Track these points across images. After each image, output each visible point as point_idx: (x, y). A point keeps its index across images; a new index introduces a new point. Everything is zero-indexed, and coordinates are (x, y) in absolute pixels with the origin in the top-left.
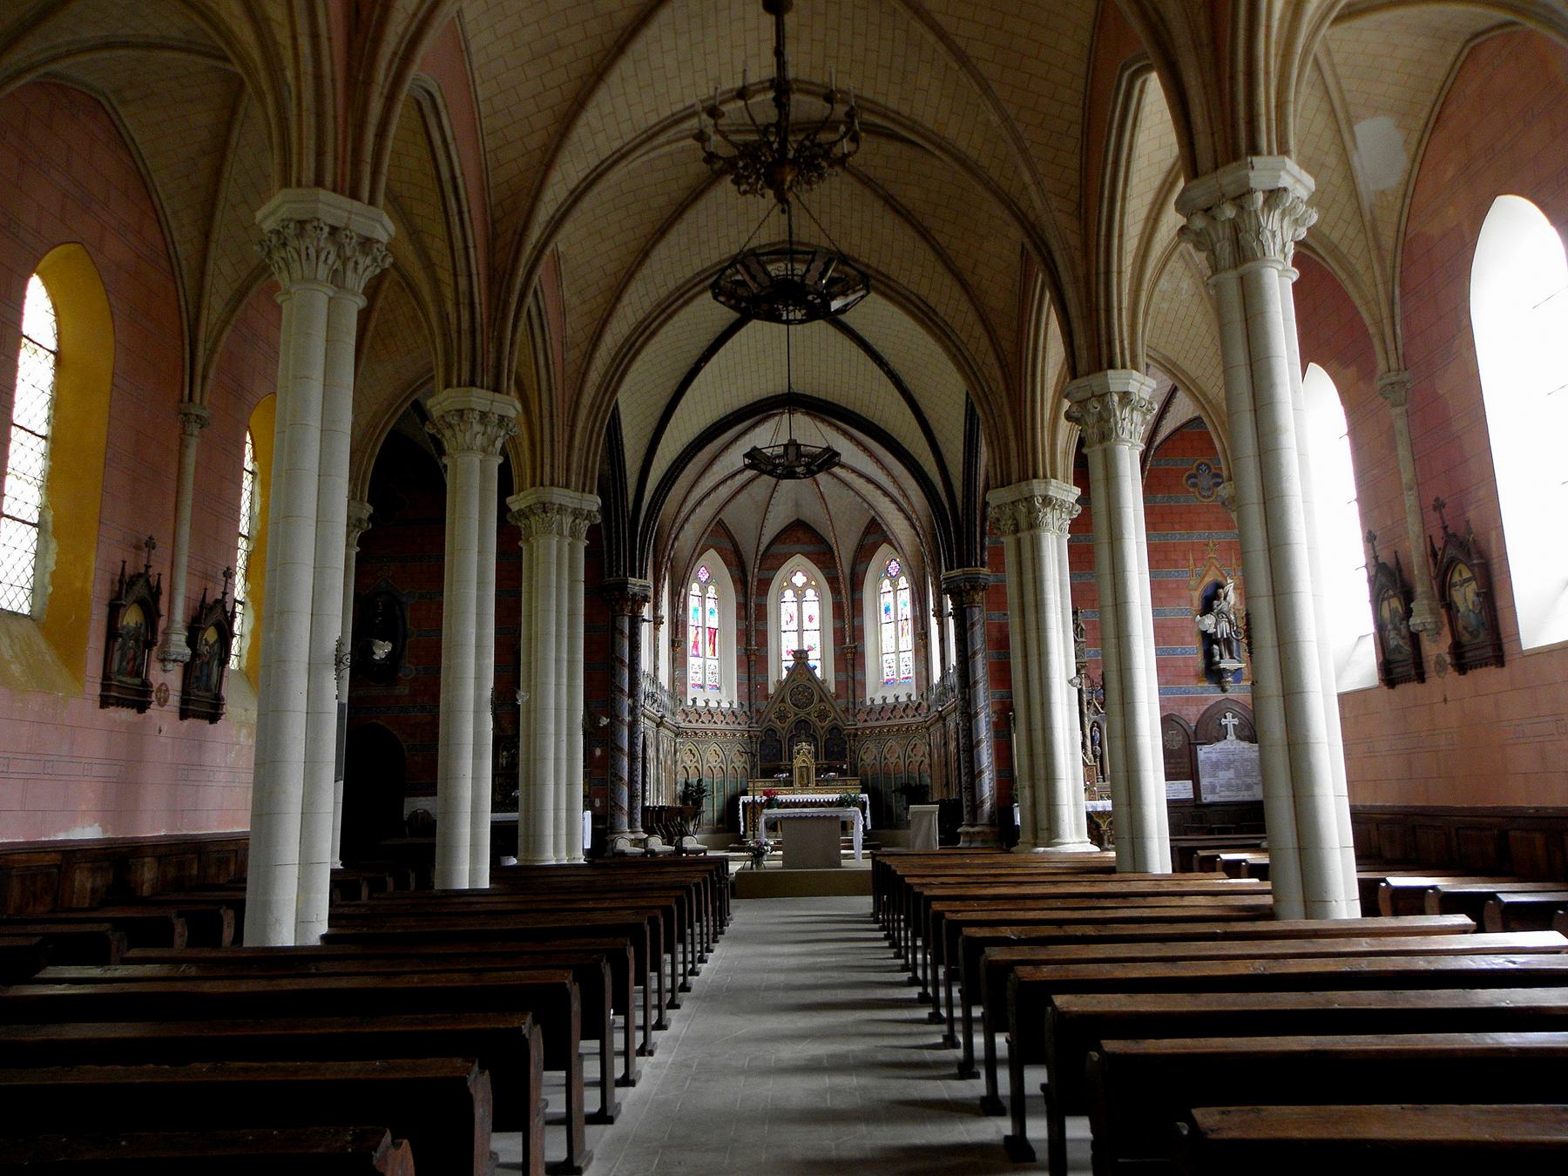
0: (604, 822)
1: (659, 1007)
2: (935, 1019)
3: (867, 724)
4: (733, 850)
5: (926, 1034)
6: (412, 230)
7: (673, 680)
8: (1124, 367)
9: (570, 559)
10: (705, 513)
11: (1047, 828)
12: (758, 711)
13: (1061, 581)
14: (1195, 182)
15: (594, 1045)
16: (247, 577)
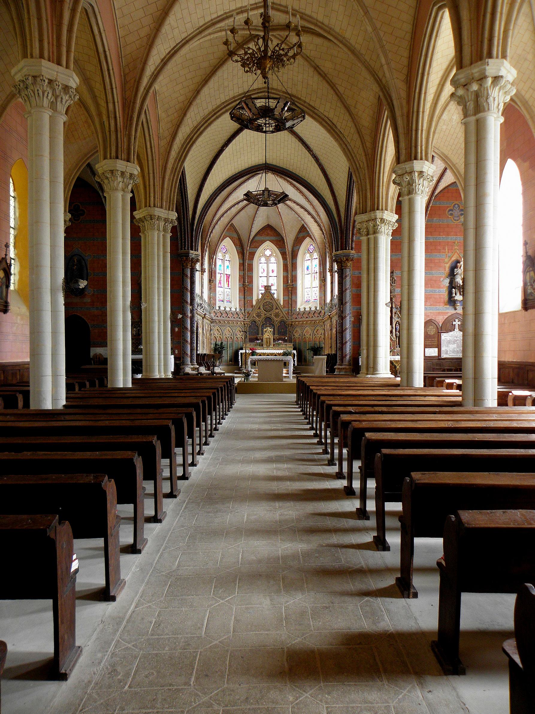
0: (180, 360)
1: (200, 445)
2: (320, 443)
3: (297, 320)
4: (236, 373)
5: (315, 448)
6: (86, 80)
7: (210, 298)
8: (421, 159)
9: (163, 242)
10: (225, 220)
11: (373, 368)
12: (248, 313)
13: (386, 258)
14: (461, 70)
15: (167, 461)
16: (15, 247)
